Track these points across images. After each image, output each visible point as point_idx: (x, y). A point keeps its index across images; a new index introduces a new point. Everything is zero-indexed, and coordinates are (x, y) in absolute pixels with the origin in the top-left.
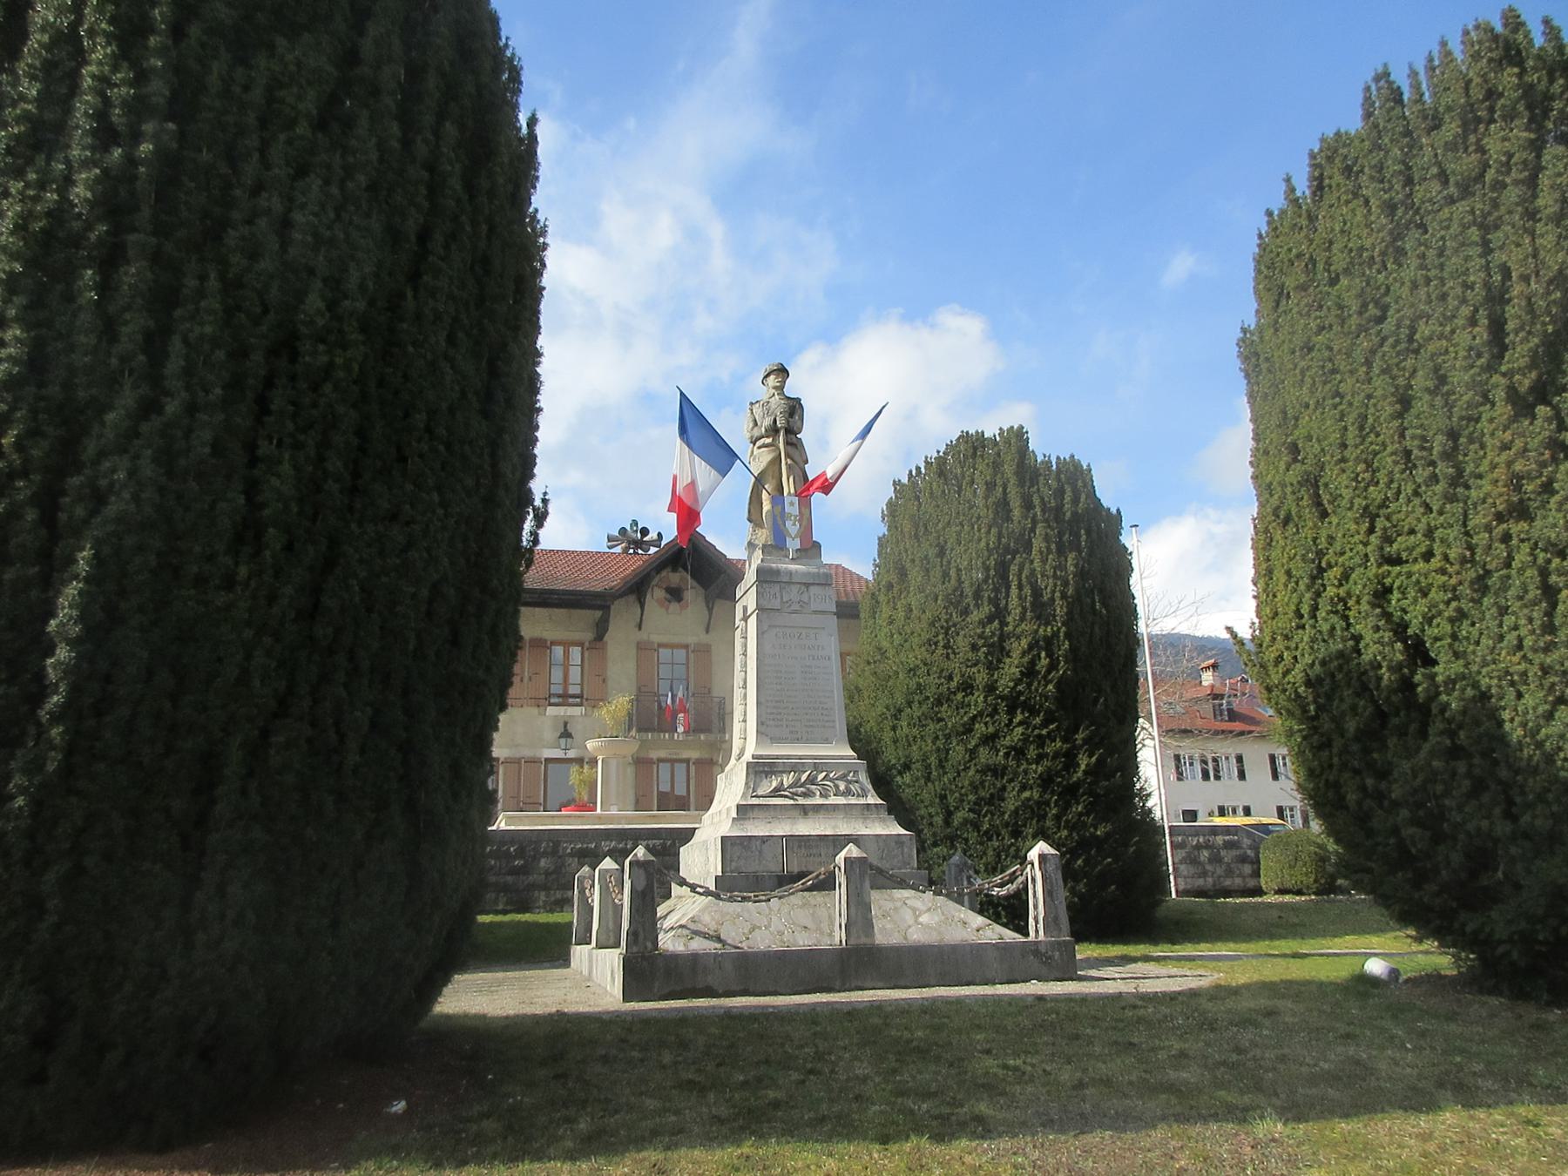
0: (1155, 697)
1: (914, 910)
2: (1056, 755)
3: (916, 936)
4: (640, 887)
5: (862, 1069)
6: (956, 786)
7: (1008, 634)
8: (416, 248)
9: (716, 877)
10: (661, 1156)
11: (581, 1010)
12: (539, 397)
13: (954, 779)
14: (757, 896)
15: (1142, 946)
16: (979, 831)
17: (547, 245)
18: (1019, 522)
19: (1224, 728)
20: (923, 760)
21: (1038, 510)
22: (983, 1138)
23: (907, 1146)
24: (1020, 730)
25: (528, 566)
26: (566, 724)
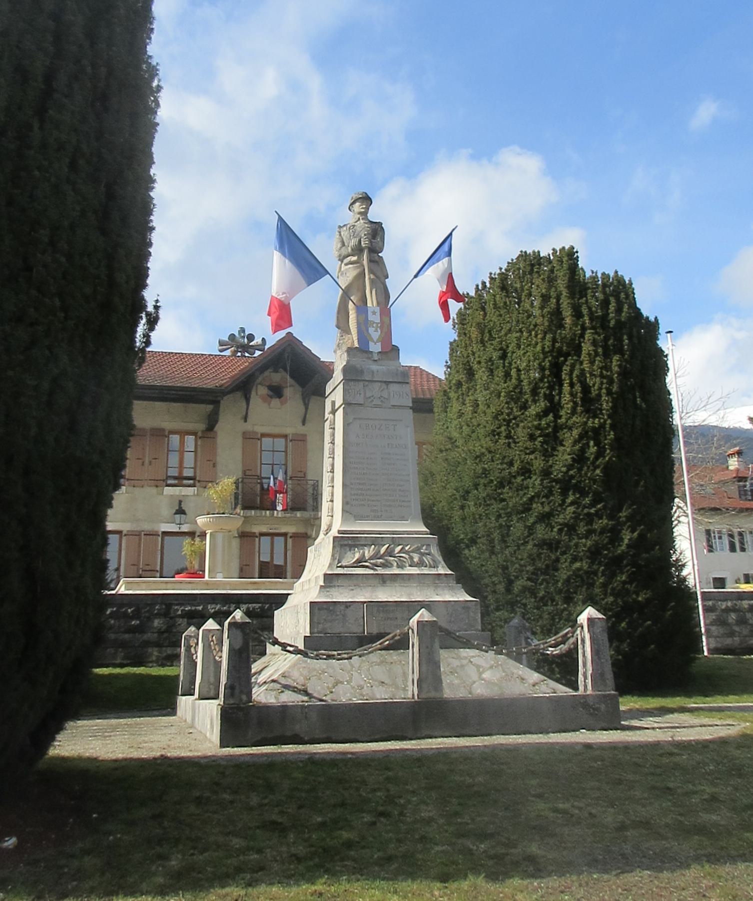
0: (689, 481)
1: (478, 667)
2: (603, 531)
3: (480, 691)
4: (238, 645)
5: (427, 812)
6: (517, 558)
7: (562, 425)
8: (43, 87)
9: (305, 637)
10: (243, 892)
11: (183, 755)
12: (152, 218)
13: (515, 552)
14: (339, 654)
15: (678, 698)
16: (536, 597)
17: (162, 88)
18: (570, 328)
19: (748, 506)
20: (488, 536)
21: (586, 318)
22: (533, 876)
23: (465, 885)
24: (571, 509)
25: (140, 366)
26: (180, 502)
